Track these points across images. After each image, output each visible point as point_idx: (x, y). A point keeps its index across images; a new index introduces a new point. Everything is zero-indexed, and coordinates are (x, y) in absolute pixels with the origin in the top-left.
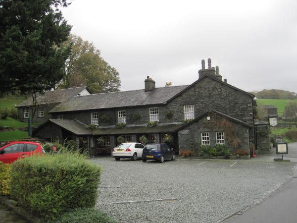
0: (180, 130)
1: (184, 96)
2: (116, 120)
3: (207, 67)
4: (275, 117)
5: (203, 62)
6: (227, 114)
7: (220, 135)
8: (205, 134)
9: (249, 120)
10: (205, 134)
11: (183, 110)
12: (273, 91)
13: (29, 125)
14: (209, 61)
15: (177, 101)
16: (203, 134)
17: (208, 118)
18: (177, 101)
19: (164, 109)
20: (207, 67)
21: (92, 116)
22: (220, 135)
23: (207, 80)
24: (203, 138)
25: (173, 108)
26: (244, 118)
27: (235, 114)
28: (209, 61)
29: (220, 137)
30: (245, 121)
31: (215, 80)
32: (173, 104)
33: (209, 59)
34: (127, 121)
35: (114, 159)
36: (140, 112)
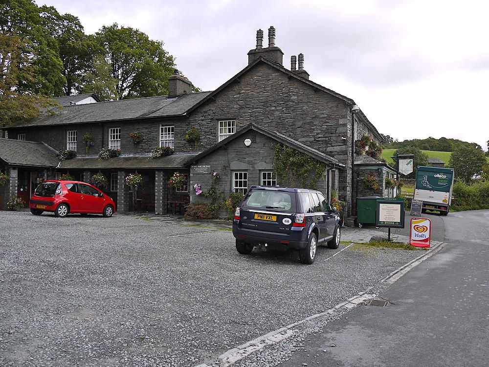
0: (192, 164)
1: (220, 102)
2: (104, 143)
3: (265, 44)
4: (410, 157)
5: (260, 34)
6: (297, 140)
7: (241, 178)
8: (241, 174)
9: (339, 153)
10: (241, 174)
11: (216, 128)
12: (443, 139)
13: (389, 235)
14: (272, 31)
15: (205, 112)
16: (236, 175)
17: (248, 142)
18: (205, 112)
19: (184, 126)
20: (265, 44)
21: (69, 136)
22: (241, 178)
23: (262, 71)
24: (236, 182)
25: (199, 122)
26: (329, 149)
27: (312, 139)
28: (272, 31)
29: (269, 182)
30: (331, 154)
31: (278, 71)
32: (199, 117)
33: (301, 54)
34: (122, 146)
35: (227, 237)
36: (143, 131)
